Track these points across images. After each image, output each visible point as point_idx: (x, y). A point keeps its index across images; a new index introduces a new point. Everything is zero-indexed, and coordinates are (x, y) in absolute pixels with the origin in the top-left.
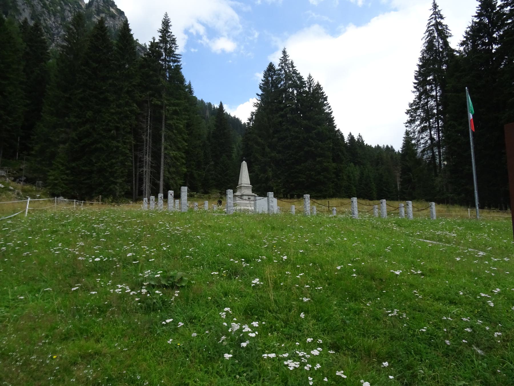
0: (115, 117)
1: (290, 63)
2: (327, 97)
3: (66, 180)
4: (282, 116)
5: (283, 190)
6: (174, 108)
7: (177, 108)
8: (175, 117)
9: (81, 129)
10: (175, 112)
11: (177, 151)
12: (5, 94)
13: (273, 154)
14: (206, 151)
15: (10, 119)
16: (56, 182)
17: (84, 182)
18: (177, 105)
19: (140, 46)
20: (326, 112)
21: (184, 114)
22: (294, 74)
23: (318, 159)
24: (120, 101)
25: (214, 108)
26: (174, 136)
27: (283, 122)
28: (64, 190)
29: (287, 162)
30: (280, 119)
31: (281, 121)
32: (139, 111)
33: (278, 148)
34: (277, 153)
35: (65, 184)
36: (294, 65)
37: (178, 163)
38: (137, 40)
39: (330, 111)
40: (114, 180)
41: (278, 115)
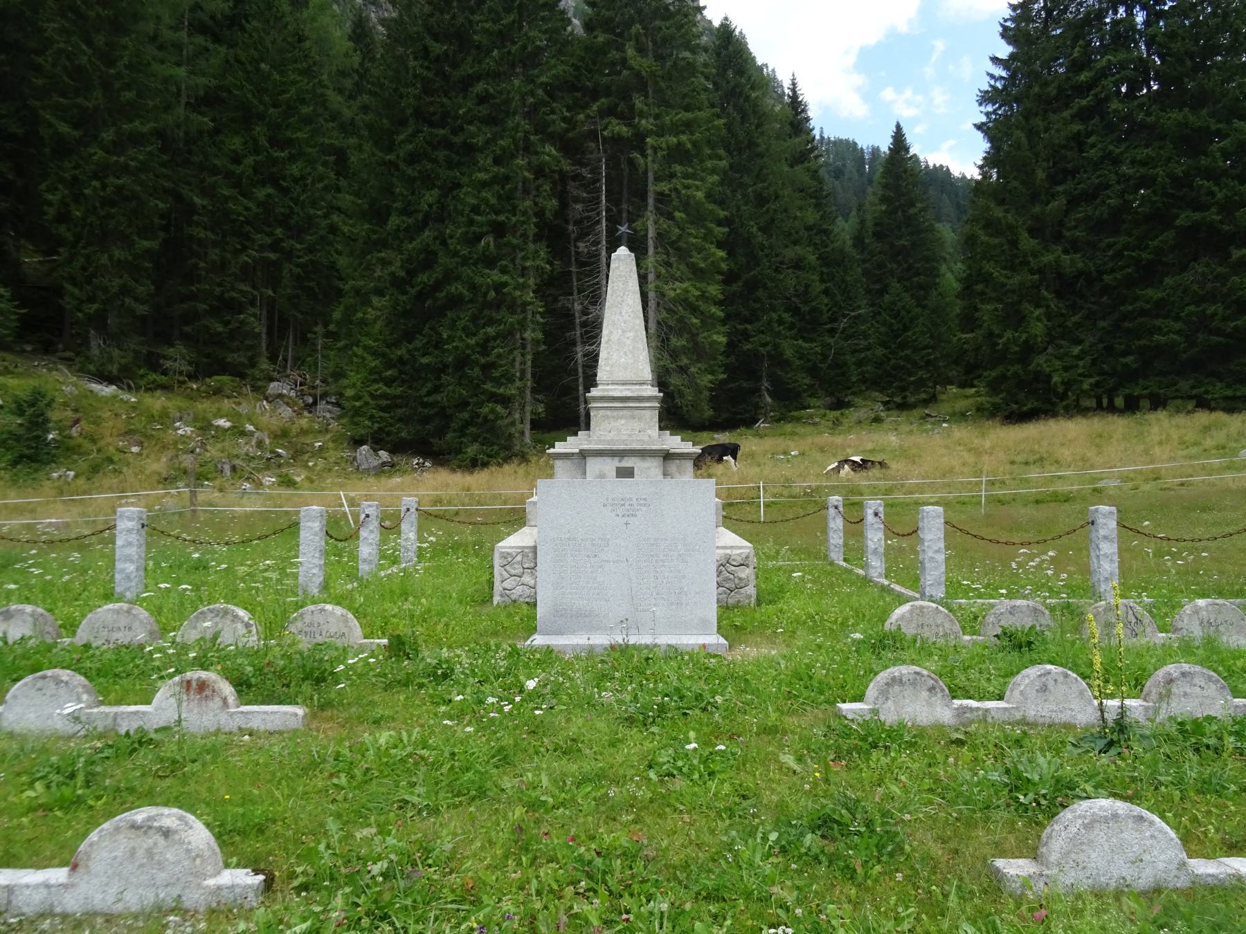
0: (489, 196)
3: (384, 396)
4: (1083, 115)
5: (1092, 380)
8: (678, 168)
9: (410, 246)
10: (678, 154)
11: (689, 279)
12: (285, 184)
13: (1048, 258)
15: (298, 246)
17: (431, 399)
18: (688, 126)
21: (710, 158)
25: (927, 166)
26: (677, 230)
27: (1089, 135)
28: (376, 425)
29: (1107, 278)
30: (1077, 127)
31: (1079, 133)
32: (566, 166)
34: (1066, 252)
35: (382, 409)
37: (695, 321)
40: (494, 390)
41: (1066, 114)
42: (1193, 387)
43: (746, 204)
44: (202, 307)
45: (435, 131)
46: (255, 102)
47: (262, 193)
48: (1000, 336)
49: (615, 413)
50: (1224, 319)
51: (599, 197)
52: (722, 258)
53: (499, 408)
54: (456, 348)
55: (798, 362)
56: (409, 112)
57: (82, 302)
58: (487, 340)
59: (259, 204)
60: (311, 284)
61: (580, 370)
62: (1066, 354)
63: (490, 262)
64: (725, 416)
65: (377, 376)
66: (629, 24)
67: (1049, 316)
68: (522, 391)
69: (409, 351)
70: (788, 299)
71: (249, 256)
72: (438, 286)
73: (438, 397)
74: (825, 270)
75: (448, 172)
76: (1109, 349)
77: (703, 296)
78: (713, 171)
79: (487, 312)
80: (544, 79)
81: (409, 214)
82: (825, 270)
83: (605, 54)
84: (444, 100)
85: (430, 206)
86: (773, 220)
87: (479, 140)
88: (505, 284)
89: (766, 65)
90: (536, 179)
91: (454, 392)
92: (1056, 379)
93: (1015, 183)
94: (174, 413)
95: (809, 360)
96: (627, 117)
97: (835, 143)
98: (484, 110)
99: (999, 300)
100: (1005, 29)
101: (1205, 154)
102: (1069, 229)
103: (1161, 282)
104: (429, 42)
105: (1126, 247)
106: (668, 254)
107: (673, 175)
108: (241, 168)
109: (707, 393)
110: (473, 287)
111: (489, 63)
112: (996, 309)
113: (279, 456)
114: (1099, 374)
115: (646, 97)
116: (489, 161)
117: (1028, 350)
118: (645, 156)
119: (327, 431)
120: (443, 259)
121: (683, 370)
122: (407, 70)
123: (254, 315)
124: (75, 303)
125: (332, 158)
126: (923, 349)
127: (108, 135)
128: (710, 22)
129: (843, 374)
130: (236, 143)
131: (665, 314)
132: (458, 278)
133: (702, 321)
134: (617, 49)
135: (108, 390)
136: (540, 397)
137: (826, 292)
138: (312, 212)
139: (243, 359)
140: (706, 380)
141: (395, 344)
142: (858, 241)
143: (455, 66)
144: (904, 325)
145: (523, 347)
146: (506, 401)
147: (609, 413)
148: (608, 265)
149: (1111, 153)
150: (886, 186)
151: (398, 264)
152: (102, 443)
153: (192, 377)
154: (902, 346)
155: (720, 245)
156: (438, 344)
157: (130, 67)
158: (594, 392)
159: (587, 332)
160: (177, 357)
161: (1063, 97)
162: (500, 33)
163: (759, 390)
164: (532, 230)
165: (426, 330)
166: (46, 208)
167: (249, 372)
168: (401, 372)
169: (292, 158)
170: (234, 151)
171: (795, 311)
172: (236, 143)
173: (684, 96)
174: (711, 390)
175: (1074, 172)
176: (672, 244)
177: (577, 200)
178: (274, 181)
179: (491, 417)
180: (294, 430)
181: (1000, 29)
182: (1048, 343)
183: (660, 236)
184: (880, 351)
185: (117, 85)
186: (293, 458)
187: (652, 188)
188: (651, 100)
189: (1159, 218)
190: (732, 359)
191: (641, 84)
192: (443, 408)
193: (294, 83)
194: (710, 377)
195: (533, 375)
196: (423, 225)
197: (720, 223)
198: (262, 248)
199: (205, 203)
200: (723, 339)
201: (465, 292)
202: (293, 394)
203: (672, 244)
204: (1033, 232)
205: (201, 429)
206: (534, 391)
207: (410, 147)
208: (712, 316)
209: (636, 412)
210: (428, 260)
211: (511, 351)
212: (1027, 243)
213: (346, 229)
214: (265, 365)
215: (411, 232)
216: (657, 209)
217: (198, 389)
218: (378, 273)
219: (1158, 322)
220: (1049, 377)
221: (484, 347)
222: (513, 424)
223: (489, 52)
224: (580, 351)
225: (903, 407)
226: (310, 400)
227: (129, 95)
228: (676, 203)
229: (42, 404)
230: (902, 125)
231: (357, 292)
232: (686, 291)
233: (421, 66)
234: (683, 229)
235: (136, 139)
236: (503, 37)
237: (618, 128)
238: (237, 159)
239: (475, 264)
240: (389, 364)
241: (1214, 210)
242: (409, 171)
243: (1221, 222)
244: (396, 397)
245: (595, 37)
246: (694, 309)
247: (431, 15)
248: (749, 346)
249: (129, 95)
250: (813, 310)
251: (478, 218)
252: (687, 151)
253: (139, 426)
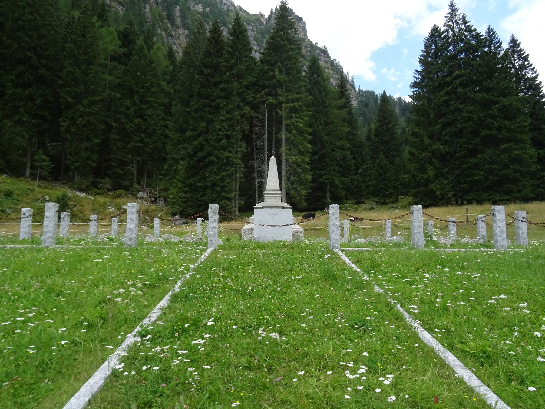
1: (461, 17)
2: (528, 55)
3: (184, 197)
4: (448, 93)
6: (292, 105)
7: (296, 104)
8: (293, 115)
9: (195, 143)
10: (294, 110)
13: (435, 147)
14: (363, 153)
15: (150, 141)
16: (175, 200)
17: (202, 199)
19: (320, 49)
20: (528, 78)
21: (306, 111)
22: (467, 32)
23: (503, 146)
24: (229, 106)
25: (405, 102)
28: (181, 209)
29: (458, 155)
30: (445, 98)
31: (447, 100)
32: (253, 114)
33: (443, 138)
34: (442, 145)
36: (467, 19)
38: (317, 43)
39: (534, 75)
41: (442, 93)
42: (488, 196)
43: (321, 125)
44: (114, 164)
45: (205, 101)
46: (135, 87)
47: (137, 121)
48: (417, 176)
50: (499, 171)
51: (264, 125)
52: (310, 148)
53: (227, 202)
54: (212, 180)
55: (341, 186)
56: (195, 94)
57: (73, 162)
58: (223, 177)
61: (257, 188)
62: (442, 183)
63: (224, 149)
64: (312, 206)
66: (276, 63)
67: (435, 168)
68: (235, 195)
69: (194, 181)
70: (338, 161)
71: (132, 145)
72: (205, 157)
73: (204, 198)
74: (354, 149)
75: (209, 116)
76: (459, 181)
77: (303, 161)
78: (307, 116)
79: (223, 167)
80: (245, 83)
81: (195, 131)
82: (354, 149)
83: (267, 73)
84: (209, 90)
85: (203, 128)
86: (331, 131)
87: (221, 105)
88: (230, 157)
89: (335, 60)
90: (242, 119)
91: (210, 196)
92: (438, 193)
93: (423, 119)
94: (108, 203)
95: (345, 185)
96: (276, 96)
97: (365, 92)
98: (223, 94)
99: (417, 163)
100: (420, 59)
101: (491, 109)
102: (443, 136)
103: (476, 156)
104: (203, 69)
105: (464, 143)
106: (290, 146)
107: (292, 117)
108: (129, 112)
109: (304, 197)
110: (218, 158)
111: (225, 77)
112: (416, 166)
113: (146, 219)
114: (455, 191)
115: (282, 89)
116: (225, 112)
117: (428, 182)
118: (281, 110)
120: (208, 148)
121: (295, 188)
122: (194, 78)
123: (133, 167)
124: (71, 162)
125: (163, 107)
126: (392, 181)
127: (85, 102)
128: (312, 42)
129: (360, 191)
130: (128, 102)
131: (289, 168)
132: (213, 154)
133: (302, 171)
134: (272, 71)
135: (83, 195)
136: (242, 198)
137: (354, 158)
138: (155, 128)
139: (128, 184)
140: (304, 192)
141: (188, 178)
142: (368, 138)
143: (212, 77)
144: (384, 172)
145: (236, 179)
146: (229, 199)
148: (268, 171)
149: (458, 108)
150: (380, 116)
151: (190, 149)
152: (85, 213)
153: (109, 190)
154: (384, 180)
155: (310, 143)
156: (205, 178)
157: (94, 77)
158: (265, 192)
159: (260, 174)
160: (107, 183)
161: (440, 87)
162: (229, 66)
163: (326, 197)
164: (240, 137)
165: (200, 173)
166: (61, 127)
167: (131, 189)
168: (190, 189)
169: (148, 108)
170: (127, 105)
171: (340, 166)
172: (128, 102)
173: (297, 88)
174: (305, 196)
175: (446, 114)
176: (291, 142)
177: (256, 126)
178: (141, 117)
179: (225, 205)
180: (150, 210)
181: (419, 60)
182: (436, 179)
183: (287, 139)
184: (375, 182)
185: (89, 83)
187: (284, 122)
188: (284, 90)
189: (475, 133)
190: (315, 185)
191: (280, 85)
193: (150, 79)
194: (305, 191)
195: (240, 190)
196: (199, 136)
197: (310, 134)
198: (136, 142)
200: (310, 177)
201: (216, 160)
202: (147, 197)
203: (291, 142)
204: (430, 137)
205: (118, 209)
206: (240, 196)
207: (196, 106)
208: (306, 169)
210: (201, 148)
211: (232, 181)
212: (427, 141)
213: (170, 136)
215: (195, 138)
216: (286, 129)
218: (182, 152)
219: (475, 171)
220: (435, 192)
221: (222, 180)
222: (232, 208)
223: (225, 73)
224: (257, 181)
225: (384, 204)
226: (153, 199)
227: (93, 87)
228: (292, 127)
229: (66, 199)
230: (386, 91)
231: (174, 159)
232: (297, 159)
233: (200, 78)
234: (295, 137)
235: (94, 103)
236: (231, 68)
237: (272, 100)
238: (128, 109)
239: (219, 150)
240: (186, 186)
241: (494, 130)
242: (195, 115)
243: (497, 134)
245: (264, 67)
246: (299, 166)
247: (204, 59)
248: (322, 180)
249: (93, 87)
250: (348, 165)
251: (221, 133)
252: (297, 108)
253: (97, 208)
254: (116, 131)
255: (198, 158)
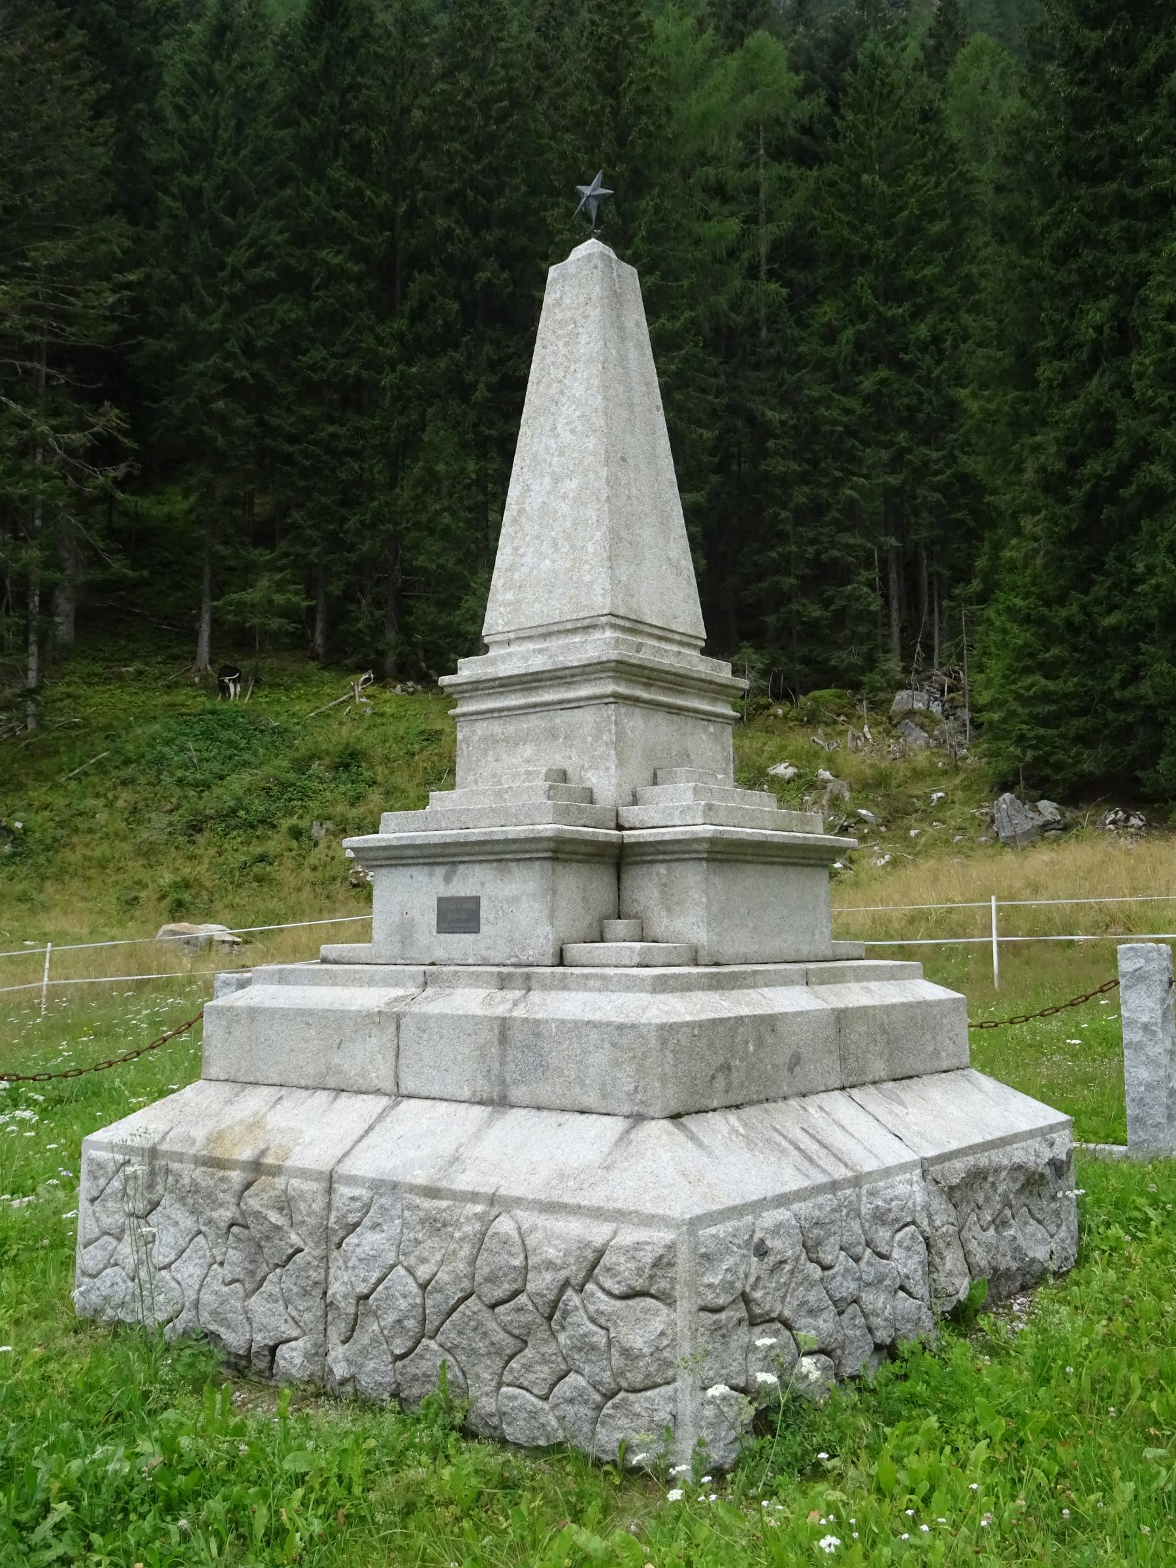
3: (1046, 697)
15: (935, 455)
28: (1030, 754)
35: (1044, 722)
49: (511, 727)
59: (867, 400)
60: (959, 515)
65: (1029, 662)
69: (1083, 607)
72: (1124, 474)
75: (1128, 259)
85: (1099, 329)
113: (862, 821)
119: (957, 769)
139: (856, 660)
147: (496, 728)
153: (781, 695)
167: (865, 679)
169: (917, 314)
186: (887, 823)
192: (1151, 709)
199: (784, 417)
202: (936, 708)
209: (561, 719)
214: (893, 665)
217: (785, 716)
238: (830, 337)
244: (1066, 696)
254: (786, 442)
255: (1088, 486)
